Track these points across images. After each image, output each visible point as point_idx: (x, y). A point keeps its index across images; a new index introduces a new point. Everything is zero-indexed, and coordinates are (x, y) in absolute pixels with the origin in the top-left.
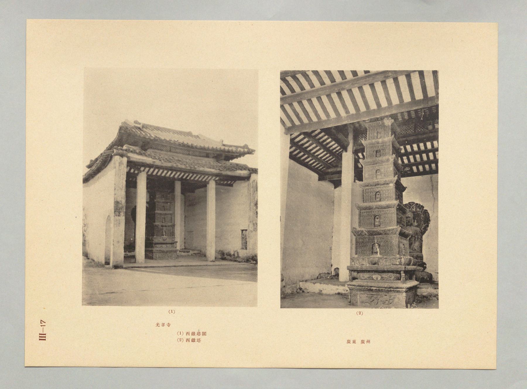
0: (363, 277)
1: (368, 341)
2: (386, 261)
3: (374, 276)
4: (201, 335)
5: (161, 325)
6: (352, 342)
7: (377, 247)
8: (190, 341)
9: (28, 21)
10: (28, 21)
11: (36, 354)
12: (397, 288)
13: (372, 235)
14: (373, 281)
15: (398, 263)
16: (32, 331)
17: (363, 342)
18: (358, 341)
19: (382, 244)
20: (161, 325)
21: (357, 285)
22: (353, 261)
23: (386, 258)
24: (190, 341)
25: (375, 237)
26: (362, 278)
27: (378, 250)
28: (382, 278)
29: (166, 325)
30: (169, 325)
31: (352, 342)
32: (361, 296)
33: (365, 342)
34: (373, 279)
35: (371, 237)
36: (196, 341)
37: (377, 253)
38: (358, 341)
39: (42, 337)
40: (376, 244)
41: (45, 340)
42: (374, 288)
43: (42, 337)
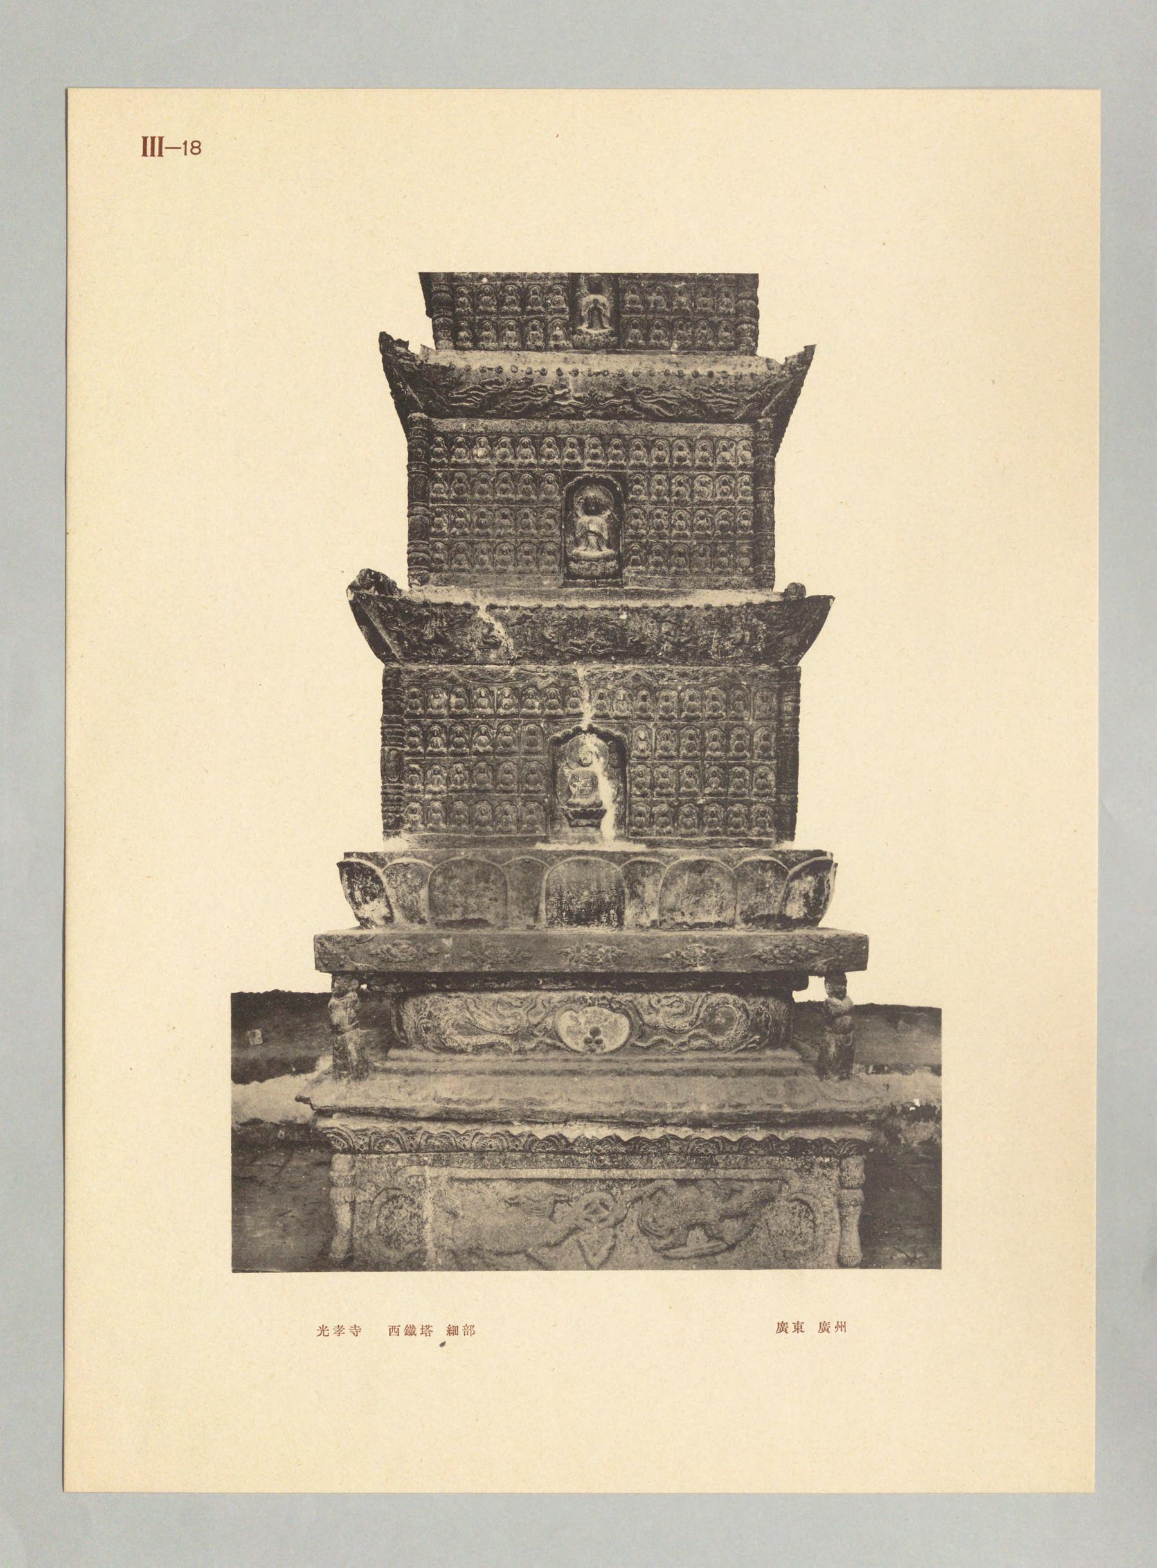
0: (470, 1029)
1: (841, 1326)
2: (699, 891)
3: (564, 1022)
4: (833, 1325)
5: (331, 1332)
6: (791, 1328)
7: (598, 767)
8: (402, 1331)
9: (1083, 108)
10: (1098, 93)
11: (104, 122)
12: (813, 1119)
13: (543, 651)
14: (554, 1061)
15: (795, 910)
16: (170, 111)
17: (824, 1327)
18: (811, 1327)
19: (641, 740)
20: (331, 1332)
21: (433, 1107)
22: (371, 895)
23: (698, 867)
24: (402, 1331)
25: (581, 671)
26: (460, 1040)
27: (606, 792)
28: (640, 1030)
29: (347, 1331)
30: (356, 1330)
31: (791, 1328)
32: (455, 1198)
33: (832, 1329)
34: (555, 1043)
35: (544, 674)
36: (418, 1331)
37: (594, 815)
38: (811, 1327)
39: (152, 147)
40: (591, 743)
41: (145, 154)
42: (594, 1132)
43: (152, 147)
